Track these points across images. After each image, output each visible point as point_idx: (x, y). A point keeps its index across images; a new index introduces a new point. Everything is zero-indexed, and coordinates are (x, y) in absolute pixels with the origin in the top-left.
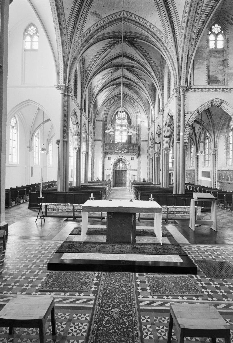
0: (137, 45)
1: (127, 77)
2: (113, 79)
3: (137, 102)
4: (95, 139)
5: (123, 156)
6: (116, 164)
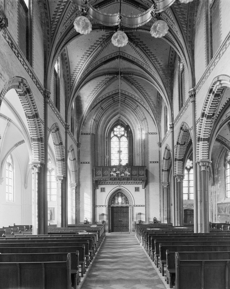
0: (132, 80)
1: (126, 56)
2: (103, 60)
3: (141, 105)
5: (122, 185)
6: (113, 198)
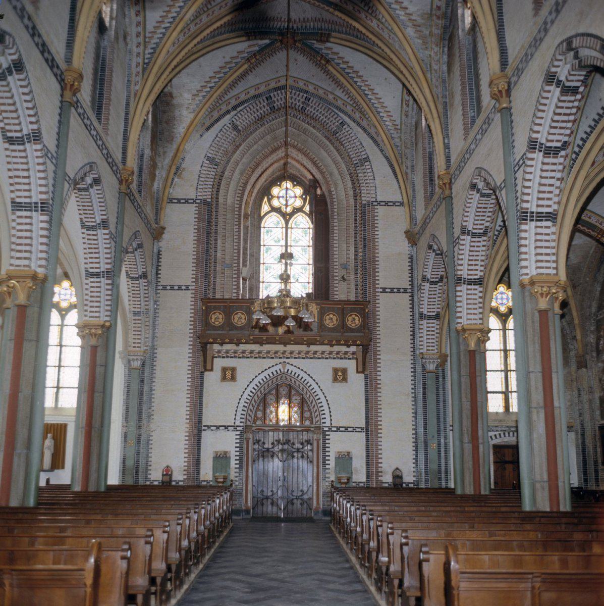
3: (354, 121)
4: (163, 282)
